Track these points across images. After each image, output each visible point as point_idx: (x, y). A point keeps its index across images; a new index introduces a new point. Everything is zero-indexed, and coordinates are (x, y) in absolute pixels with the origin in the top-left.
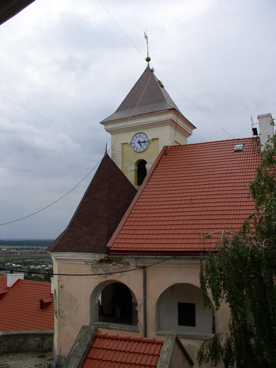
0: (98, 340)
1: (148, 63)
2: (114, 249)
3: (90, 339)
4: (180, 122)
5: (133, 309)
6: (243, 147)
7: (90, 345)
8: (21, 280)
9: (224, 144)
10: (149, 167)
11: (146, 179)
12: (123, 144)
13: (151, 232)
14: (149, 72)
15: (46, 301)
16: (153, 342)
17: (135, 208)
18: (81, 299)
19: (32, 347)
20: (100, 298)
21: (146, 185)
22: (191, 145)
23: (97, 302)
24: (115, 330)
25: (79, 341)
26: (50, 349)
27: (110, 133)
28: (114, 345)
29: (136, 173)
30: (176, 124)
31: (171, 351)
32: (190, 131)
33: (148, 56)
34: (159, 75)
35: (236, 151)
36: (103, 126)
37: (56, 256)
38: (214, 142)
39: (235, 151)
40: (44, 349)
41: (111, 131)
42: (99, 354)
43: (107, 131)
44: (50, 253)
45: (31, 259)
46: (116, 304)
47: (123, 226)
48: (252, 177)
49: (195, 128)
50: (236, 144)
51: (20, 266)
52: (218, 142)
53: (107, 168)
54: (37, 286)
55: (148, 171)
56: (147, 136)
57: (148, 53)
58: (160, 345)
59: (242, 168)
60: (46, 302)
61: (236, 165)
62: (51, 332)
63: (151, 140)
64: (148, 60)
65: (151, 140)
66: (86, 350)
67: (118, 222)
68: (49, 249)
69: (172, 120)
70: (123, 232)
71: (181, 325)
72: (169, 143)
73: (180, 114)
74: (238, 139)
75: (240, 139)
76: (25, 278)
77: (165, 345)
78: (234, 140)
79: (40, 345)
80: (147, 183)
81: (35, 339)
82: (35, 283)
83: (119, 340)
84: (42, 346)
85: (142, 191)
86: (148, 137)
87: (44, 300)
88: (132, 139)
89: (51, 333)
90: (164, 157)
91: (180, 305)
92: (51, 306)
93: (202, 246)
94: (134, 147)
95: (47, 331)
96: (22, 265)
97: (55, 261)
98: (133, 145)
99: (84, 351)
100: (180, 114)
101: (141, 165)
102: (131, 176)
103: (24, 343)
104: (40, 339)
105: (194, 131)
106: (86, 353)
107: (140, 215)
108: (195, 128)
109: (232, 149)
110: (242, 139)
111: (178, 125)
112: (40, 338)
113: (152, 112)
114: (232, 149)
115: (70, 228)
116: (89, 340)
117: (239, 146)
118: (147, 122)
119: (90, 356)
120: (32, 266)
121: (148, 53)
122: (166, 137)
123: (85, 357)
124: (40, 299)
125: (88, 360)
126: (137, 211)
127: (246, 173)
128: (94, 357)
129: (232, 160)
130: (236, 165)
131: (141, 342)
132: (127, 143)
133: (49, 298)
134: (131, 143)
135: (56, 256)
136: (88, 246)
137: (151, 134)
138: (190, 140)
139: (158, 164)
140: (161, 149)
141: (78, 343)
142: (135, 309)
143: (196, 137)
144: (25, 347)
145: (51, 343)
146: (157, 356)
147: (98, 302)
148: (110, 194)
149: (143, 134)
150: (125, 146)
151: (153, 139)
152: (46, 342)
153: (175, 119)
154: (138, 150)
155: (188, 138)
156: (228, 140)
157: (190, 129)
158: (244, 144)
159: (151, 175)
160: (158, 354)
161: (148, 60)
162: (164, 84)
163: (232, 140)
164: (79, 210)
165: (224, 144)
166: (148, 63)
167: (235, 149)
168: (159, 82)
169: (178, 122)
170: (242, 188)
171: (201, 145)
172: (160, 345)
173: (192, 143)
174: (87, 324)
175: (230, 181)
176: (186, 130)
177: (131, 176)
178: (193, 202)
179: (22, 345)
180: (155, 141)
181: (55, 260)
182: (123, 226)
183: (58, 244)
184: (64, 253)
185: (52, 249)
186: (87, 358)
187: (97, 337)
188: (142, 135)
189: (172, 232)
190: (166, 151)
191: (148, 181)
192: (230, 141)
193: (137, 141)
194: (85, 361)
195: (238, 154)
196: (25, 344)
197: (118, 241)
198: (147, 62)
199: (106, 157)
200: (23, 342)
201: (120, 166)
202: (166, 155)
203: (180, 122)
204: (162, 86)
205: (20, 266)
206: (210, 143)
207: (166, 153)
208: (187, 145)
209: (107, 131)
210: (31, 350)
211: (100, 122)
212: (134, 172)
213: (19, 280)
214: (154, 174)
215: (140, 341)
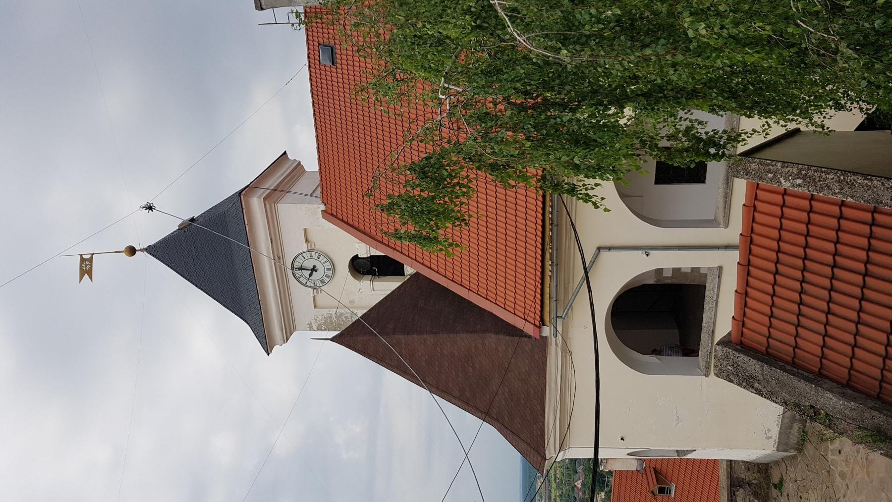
2: (538, 318)
4: (272, 183)
5: (669, 282)
10: (364, 250)
12: (315, 307)
14: (164, 251)
26: (762, 468)
30: (274, 190)
34: (163, 226)
43: (287, 340)
44: (547, 464)
46: (658, 318)
61: (350, 132)
62: (725, 466)
64: (132, 251)
88: (305, 285)
91: (658, 181)
94: (322, 281)
95: (724, 482)
98: (319, 284)
101: (359, 267)
102: (387, 286)
105: (291, 156)
130: (350, 132)
132: (314, 298)
137: (294, 246)
138: (311, 164)
143: (306, 152)
145: (749, 465)
151: (307, 240)
152: (744, 475)
153: (263, 193)
157: (288, 165)
161: (132, 251)
167: (329, 64)
171: (321, 148)
177: (387, 286)
190: (330, 214)
193: (319, 266)
201: (365, 311)
212: (375, 283)
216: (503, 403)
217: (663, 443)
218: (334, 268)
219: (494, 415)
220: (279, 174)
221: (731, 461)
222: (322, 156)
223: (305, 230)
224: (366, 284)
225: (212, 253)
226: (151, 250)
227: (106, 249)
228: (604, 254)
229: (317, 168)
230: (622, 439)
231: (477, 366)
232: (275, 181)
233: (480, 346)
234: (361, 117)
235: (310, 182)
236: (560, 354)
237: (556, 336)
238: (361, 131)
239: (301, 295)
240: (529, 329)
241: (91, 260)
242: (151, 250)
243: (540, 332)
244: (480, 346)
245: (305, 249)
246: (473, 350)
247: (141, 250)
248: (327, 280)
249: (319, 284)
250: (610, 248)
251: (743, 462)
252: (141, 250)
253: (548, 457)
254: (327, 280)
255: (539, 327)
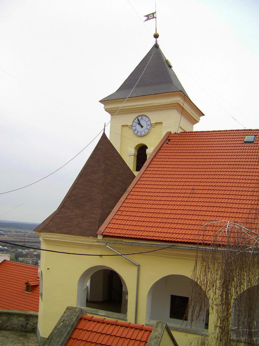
0: (83, 322)
1: (156, 39)
2: (107, 234)
3: (74, 320)
4: (187, 107)
6: (254, 138)
7: (75, 326)
8: (7, 261)
9: (233, 134)
10: (149, 151)
11: (146, 164)
12: (123, 126)
13: (132, 228)
15: (32, 284)
16: (141, 329)
17: (131, 193)
18: (249, 317)
19: (16, 326)
20: (88, 284)
21: (145, 170)
22: (197, 132)
23: (85, 287)
24: (101, 314)
25: (63, 321)
26: (34, 330)
27: (110, 113)
28: (100, 328)
29: (136, 158)
30: (183, 108)
31: (159, 338)
32: (198, 118)
33: (156, 32)
34: (168, 53)
35: (246, 142)
36: (102, 106)
37: (45, 237)
38: (222, 131)
39: (245, 142)
40: (28, 329)
41: (110, 112)
42: (85, 336)
43: (107, 111)
45: (20, 244)
46: (107, 290)
47: (117, 211)
48: (255, 174)
49: (203, 115)
50: (247, 135)
51: (7, 248)
52: (227, 131)
53: (104, 149)
54: (24, 269)
55: (148, 156)
56: (148, 118)
57: (156, 28)
58: (149, 332)
59: (254, 158)
60: (32, 285)
63: (154, 124)
64: (156, 36)
65: (154, 124)
66: (70, 331)
67: (113, 207)
68: (37, 229)
69: (178, 104)
70: (117, 217)
71: (172, 318)
72: (174, 130)
73: (188, 98)
74: (250, 130)
75: (251, 130)
76: (11, 259)
77: (154, 333)
78: (245, 130)
79: (24, 325)
80: (146, 169)
81: (19, 319)
82: (23, 265)
83: (105, 324)
84: (28, 327)
85: (140, 177)
86: (151, 120)
87: (30, 283)
89: (36, 315)
90: (165, 145)
91: (172, 296)
92: (37, 289)
93: (201, 238)
94: (135, 130)
95: (31, 313)
96: (10, 248)
97: (43, 242)
99: (68, 331)
100: (188, 98)
101: (141, 150)
102: (130, 162)
103: (8, 322)
104: (24, 320)
105: (202, 118)
106: (70, 333)
107: (137, 201)
108: (203, 115)
109: (242, 139)
110: (254, 130)
111: (184, 110)
112: (24, 319)
113: (157, 94)
114: (242, 139)
115: (60, 210)
116: (74, 321)
117: (248, 138)
118: (151, 104)
119: (74, 337)
120: (19, 249)
121: (156, 28)
122: (172, 123)
123: (69, 337)
124: (26, 281)
125: (72, 340)
126: (134, 197)
127: (255, 166)
128: (78, 337)
129: (230, 157)
131: (128, 327)
132: (127, 126)
133: (35, 281)
134: (132, 126)
135: (45, 237)
136: (79, 229)
137: (154, 117)
138: (197, 128)
139: (160, 149)
140: (164, 133)
141: (61, 324)
142: (125, 297)
144: (8, 325)
146: (144, 342)
147: (86, 287)
148: (103, 179)
149: (145, 117)
150: (126, 129)
151: (156, 123)
153: (182, 103)
154: (139, 134)
155: (195, 126)
156: (238, 130)
157: (197, 117)
158: (256, 136)
159: (152, 161)
160: (145, 340)
161: (156, 36)
162: (172, 63)
163: (243, 130)
164: (72, 191)
165: (233, 134)
166: (156, 39)
168: (167, 61)
169: (185, 106)
170: (249, 181)
172: (149, 332)
173: (199, 131)
174: (74, 305)
175: (246, 170)
176: (194, 117)
177: (130, 162)
178: (195, 191)
179: (6, 323)
180: (158, 127)
181: (43, 241)
182: (117, 211)
183: (47, 225)
184: (53, 235)
185: (40, 230)
186: (70, 338)
187: (83, 319)
188: (144, 118)
189: (149, 229)
190: (169, 138)
191: (147, 167)
192: (241, 132)
194: (68, 340)
195: (248, 145)
196: (9, 322)
197: (111, 226)
198: (155, 39)
199: (104, 136)
200: (6, 320)
202: (169, 141)
203: (187, 107)
204: (170, 67)
205: (7, 248)
206: (218, 131)
207: (169, 139)
208: (193, 132)
209: (107, 110)
210: (15, 329)
211: (100, 100)
213: (5, 260)
214: (155, 160)
215: (128, 326)
216: (68, 215)
217: (46, 286)
218: (141, 136)
219: (61, 210)
220: (193, 112)
221: (38, 317)
222: (200, 133)
223: (161, 123)
224: (132, 151)
225: (153, 77)
226: (156, 46)
227: (160, 24)
228: (136, 269)
229: (194, 130)
230: (48, 269)
231: (86, 203)
232: (188, 109)
233: (95, 205)
234: (249, 160)
235: (187, 127)
236: (89, 243)
237: (97, 242)
238: (241, 160)
239: (129, 120)
240: (102, 229)
241: (154, 17)
242: (156, 46)
243: (100, 234)
244: (95, 205)
245: (152, 122)
246: (94, 202)
247: (156, 41)
248: (136, 132)
250: (139, 271)
251: (37, 322)
252: (156, 41)
253: (41, 233)
254: (136, 132)
255: (102, 234)
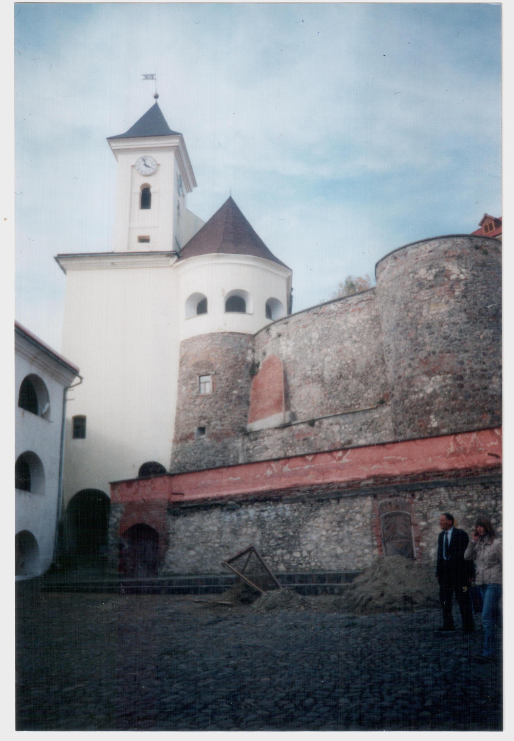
94: (139, 169)
248: (140, 171)
249: (137, 168)
254: (140, 171)
